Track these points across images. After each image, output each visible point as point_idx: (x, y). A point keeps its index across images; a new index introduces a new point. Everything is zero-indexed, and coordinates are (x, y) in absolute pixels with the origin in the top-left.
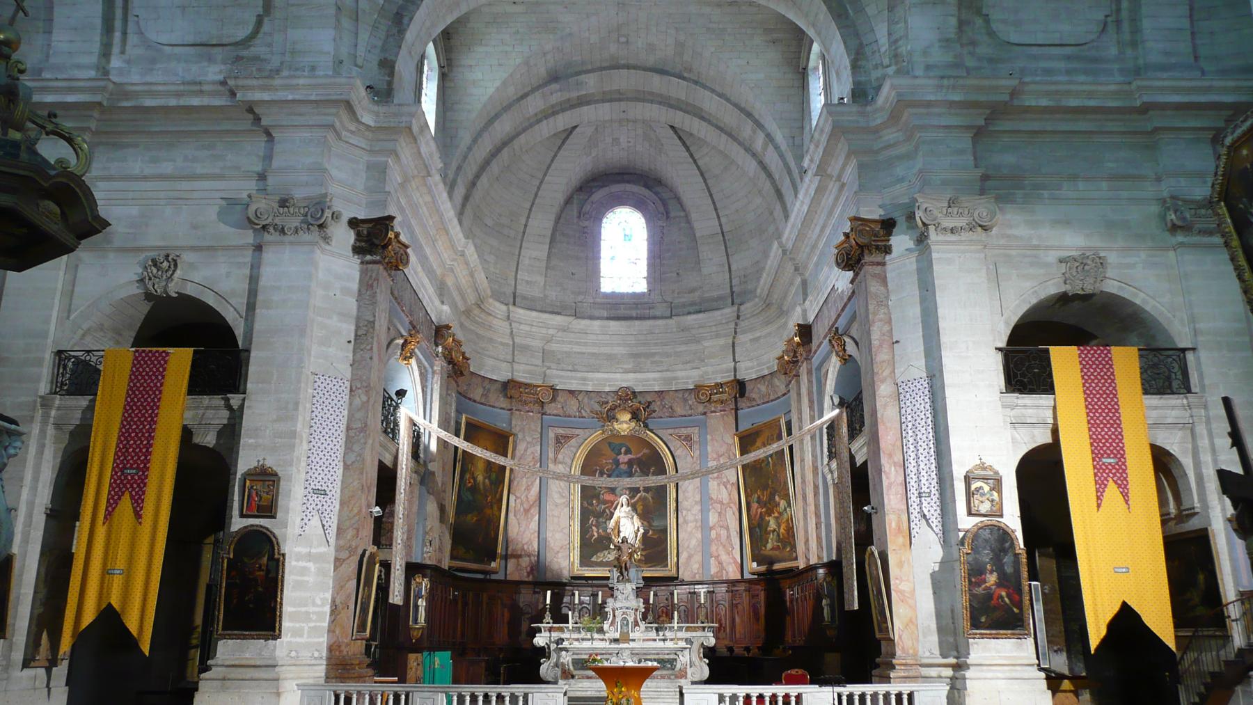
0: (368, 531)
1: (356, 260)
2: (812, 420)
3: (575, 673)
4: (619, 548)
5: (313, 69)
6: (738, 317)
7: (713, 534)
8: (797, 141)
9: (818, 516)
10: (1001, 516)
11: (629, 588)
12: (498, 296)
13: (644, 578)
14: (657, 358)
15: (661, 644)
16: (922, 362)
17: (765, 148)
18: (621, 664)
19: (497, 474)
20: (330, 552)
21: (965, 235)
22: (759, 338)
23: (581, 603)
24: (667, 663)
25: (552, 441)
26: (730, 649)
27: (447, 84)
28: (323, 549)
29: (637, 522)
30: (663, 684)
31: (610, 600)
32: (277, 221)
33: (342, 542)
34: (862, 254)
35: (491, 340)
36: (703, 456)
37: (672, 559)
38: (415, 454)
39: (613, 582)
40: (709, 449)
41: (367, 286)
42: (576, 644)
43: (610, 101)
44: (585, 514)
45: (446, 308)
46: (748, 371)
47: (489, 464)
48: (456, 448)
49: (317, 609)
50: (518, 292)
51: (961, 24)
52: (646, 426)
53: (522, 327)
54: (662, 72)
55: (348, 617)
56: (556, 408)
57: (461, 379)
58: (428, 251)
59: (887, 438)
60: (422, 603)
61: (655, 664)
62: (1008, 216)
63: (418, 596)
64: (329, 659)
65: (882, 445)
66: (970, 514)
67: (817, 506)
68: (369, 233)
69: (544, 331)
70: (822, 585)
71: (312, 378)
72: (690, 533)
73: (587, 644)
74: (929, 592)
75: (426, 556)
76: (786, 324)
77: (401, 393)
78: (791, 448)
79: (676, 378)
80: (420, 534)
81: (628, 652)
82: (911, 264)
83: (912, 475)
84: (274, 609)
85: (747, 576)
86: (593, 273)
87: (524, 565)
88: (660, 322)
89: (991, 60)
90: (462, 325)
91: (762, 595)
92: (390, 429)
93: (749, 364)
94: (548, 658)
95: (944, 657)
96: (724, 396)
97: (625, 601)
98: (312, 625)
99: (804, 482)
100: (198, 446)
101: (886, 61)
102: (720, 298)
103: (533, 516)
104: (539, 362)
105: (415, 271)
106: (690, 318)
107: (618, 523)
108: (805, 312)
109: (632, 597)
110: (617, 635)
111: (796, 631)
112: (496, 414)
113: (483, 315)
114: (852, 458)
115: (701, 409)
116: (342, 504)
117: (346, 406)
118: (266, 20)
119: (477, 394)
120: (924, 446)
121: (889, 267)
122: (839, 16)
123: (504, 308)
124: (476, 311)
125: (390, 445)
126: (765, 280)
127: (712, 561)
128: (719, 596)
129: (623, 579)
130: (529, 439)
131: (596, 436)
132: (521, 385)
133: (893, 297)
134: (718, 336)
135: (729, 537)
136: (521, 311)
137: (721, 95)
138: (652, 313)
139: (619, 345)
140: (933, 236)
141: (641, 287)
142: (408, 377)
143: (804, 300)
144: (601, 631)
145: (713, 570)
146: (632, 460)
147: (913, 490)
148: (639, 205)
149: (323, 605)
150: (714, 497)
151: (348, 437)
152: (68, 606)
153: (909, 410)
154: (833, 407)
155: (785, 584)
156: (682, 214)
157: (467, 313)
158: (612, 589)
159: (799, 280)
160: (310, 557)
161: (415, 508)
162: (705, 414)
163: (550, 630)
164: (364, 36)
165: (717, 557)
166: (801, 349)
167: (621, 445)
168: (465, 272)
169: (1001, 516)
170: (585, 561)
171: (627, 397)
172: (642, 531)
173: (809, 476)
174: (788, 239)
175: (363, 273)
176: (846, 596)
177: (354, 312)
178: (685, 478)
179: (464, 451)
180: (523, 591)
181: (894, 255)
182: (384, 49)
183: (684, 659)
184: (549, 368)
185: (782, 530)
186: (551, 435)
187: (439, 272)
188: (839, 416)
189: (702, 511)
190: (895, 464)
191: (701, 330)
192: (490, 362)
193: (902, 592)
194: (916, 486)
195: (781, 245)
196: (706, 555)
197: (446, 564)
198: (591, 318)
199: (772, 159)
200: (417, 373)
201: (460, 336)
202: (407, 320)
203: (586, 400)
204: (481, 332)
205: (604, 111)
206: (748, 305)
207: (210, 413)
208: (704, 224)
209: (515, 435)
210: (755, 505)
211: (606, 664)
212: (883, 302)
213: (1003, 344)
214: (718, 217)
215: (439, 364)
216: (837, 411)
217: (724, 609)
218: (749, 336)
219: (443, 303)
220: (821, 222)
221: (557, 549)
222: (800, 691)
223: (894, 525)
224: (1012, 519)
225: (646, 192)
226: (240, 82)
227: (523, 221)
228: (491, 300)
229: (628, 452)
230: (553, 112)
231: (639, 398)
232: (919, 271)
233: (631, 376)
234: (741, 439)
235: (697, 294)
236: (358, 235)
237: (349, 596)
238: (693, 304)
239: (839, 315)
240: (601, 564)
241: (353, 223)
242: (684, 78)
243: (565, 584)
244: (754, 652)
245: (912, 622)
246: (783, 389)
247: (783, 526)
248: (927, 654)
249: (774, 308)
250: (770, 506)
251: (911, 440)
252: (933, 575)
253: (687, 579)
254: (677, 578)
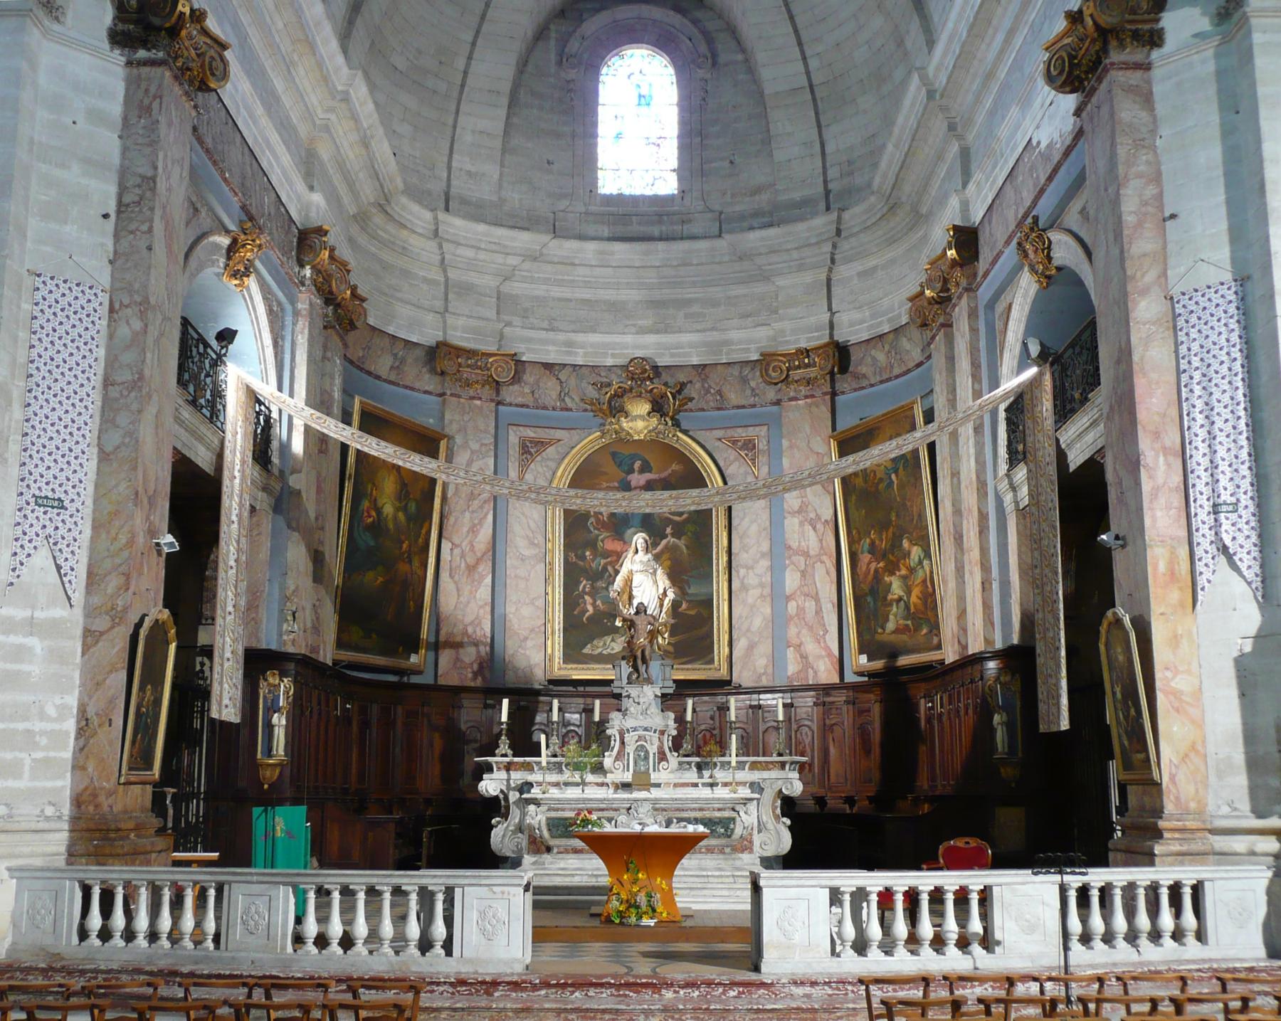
0: (152, 579)
1: (117, 58)
2: (977, 394)
3: (552, 842)
4: (630, 624)
6: (839, 232)
7: (792, 607)
9: (985, 568)
11: (649, 693)
13: (675, 681)
14: (696, 308)
15: (705, 793)
18: (638, 828)
19: (419, 493)
20: (74, 618)
22: (874, 269)
23: (566, 724)
24: (721, 826)
25: (514, 451)
26: (820, 801)
28: (60, 612)
29: (663, 582)
30: (710, 861)
31: (615, 717)
33: (96, 600)
34: (1105, 50)
35: (406, 273)
37: (721, 649)
39: (621, 685)
41: (140, 109)
42: (554, 793)
44: (572, 575)
45: (317, 198)
46: (853, 329)
48: (344, 448)
49: (49, 726)
50: (453, 191)
52: (677, 424)
53: (461, 251)
55: (112, 742)
56: (523, 395)
57: (351, 337)
58: (279, 85)
59: (1152, 402)
60: (279, 721)
61: (701, 829)
63: (273, 708)
64: (74, 820)
65: (1142, 415)
67: (984, 551)
69: (499, 259)
70: (992, 690)
71: (29, 281)
72: (752, 607)
73: (573, 793)
74: (1233, 692)
75: (288, 637)
76: (925, 238)
77: (227, 336)
78: (932, 447)
79: (727, 343)
80: (266, 596)
81: (646, 807)
82: (1205, 63)
83: (1200, 471)
85: (850, 678)
86: (586, 163)
87: (467, 660)
88: (702, 245)
90: (351, 240)
91: (876, 709)
92: (212, 408)
93: (856, 315)
94: (506, 816)
95: (1260, 816)
96: (812, 372)
97: (642, 716)
98: (39, 755)
99: (958, 512)
102: (805, 203)
103: (482, 578)
104: (491, 314)
105: (237, 90)
106: (753, 235)
107: (629, 582)
108: (965, 207)
109: (655, 709)
110: (628, 777)
111: (941, 764)
112: (418, 400)
113: (391, 228)
114: (1061, 456)
115: (771, 394)
116: (96, 527)
117: (102, 339)
119: (383, 365)
120: (1226, 414)
121: (1157, 73)
123: (428, 215)
124: (378, 219)
125: (205, 430)
126: (891, 157)
127: (790, 653)
129: (638, 677)
130: (475, 446)
131: (589, 442)
132: (459, 351)
133: (1165, 131)
134: (801, 268)
135: (819, 611)
136: (458, 222)
138: (687, 229)
141: (668, 185)
142: (246, 312)
143: (965, 185)
144: (599, 769)
145: (792, 668)
146: (651, 459)
147: (1202, 500)
148: (664, 42)
149: (61, 718)
150: (795, 545)
151: (106, 400)
153: (1195, 347)
154: (1024, 359)
156: (740, 57)
157: (361, 219)
158: (618, 697)
159: (954, 148)
161: (264, 553)
162: (778, 403)
163: (508, 767)
165: (799, 646)
166: (958, 273)
167: (634, 457)
168: (354, 137)
170: (573, 652)
171: (644, 376)
172: (671, 595)
173: (970, 499)
174: (938, 69)
175: (132, 84)
176: (1042, 707)
177: (116, 159)
179: (359, 453)
180: (466, 703)
183: (748, 818)
184: (508, 324)
185: (914, 599)
186: (513, 438)
187: (303, 130)
188: (1035, 383)
189: (772, 568)
190: (1165, 451)
191: (775, 258)
192: (404, 311)
193: (1176, 694)
194: (1207, 491)
195: (924, 79)
196: (780, 642)
197: (327, 654)
198: (582, 237)
200: (258, 298)
201: (344, 252)
202: (235, 201)
203: (573, 382)
206: (857, 210)
208: (778, 71)
209: (450, 438)
210: (865, 558)
211: (609, 828)
212: (1146, 142)
214: (804, 58)
215: (306, 300)
216: (1033, 370)
217: (808, 736)
218: (858, 266)
219: (311, 188)
220: (1007, 23)
221: (524, 633)
222: (988, 881)
223: (1162, 567)
225: (675, 19)
227: (460, 63)
228: (404, 200)
229: (645, 468)
231: (665, 377)
233: (651, 339)
235: (764, 197)
237: (111, 701)
239: (1041, 192)
243: (537, 693)
244: (862, 805)
245: (1195, 750)
246: (917, 355)
247: (916, 592)
248: (1225, 810)
249: (903, 210)
250: (892, 558)
251: (1199, 404)
252: (1242, 665)
254: (729, 682)
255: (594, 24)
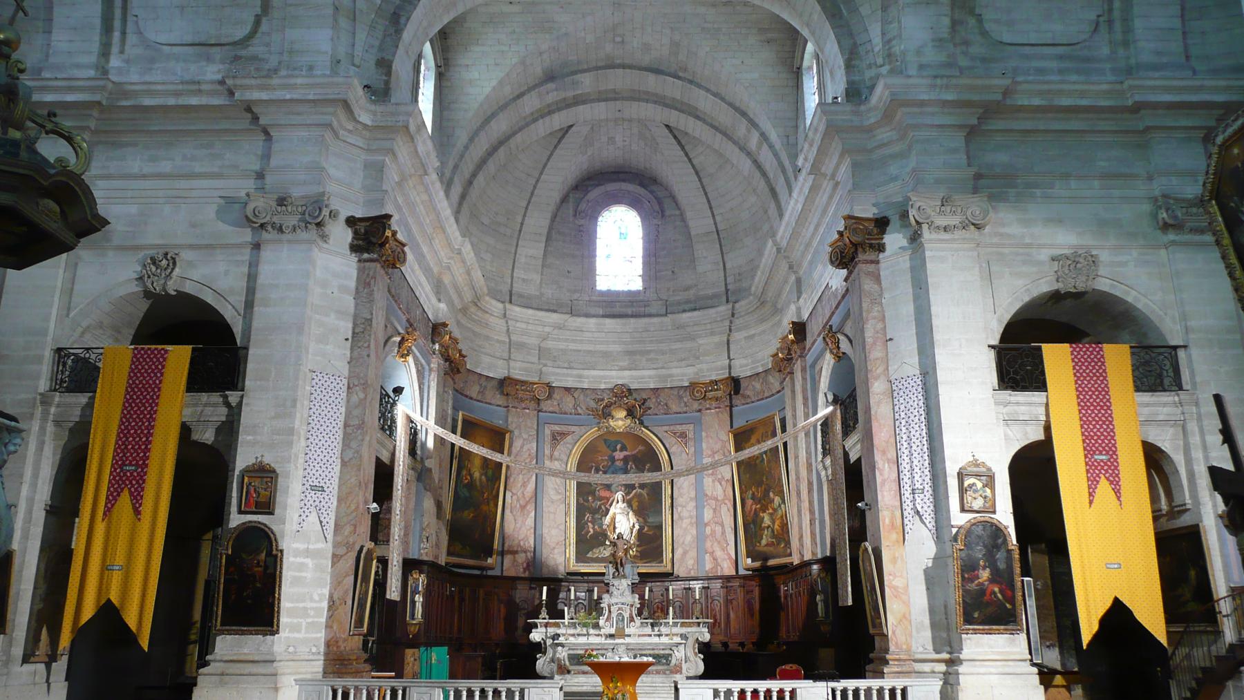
0: (365, 527)
1: (354, 258)
2: (807, 417)
3: (571, 668)
4: (614, 544)
5: (311, 68)
6: (733, 315)
7: (708, 530)
8: (792, 140)
9: (812, 512)
10: (994, 512)
11: (624, 584)
12: (494, 294)
13: (639, 574)
14: (652, 356)
15: (656, 640)
16: (915, 360)
17: (759, 147)
18: (617, 659)
19: (493, 471)
20: (328, 548)
21: (959, 234)
22: (754, 335)
23: (577, 598)
24: (662, 659)
25: (548, 438)
26: (725, 645)
27: (444, 84)
28: (321, 545)
29: (633, 518)
30: (658, 679)
31: (606, 596)
32: (275, 219)
33: (339, 539)
34: (856, 252)
35: (487, 338)
36: (698, 453)
37: (667, 555)
38: (412, 451)
39: (609, 578)
40: (704, 445)
41: (364, 284)
42: (572, 640)
43: (606, 100)
44: (581, 511)
45: (442, 306)
46: (742, 369)
47: (485, 461)
48: (453, 445)
49: (314, 605)
50: (515, 290)
51: (954, 24)
52: (641, 423)
53: (518, 325)
54: (657, 71)
55: (346, 613)
56: (552, 406)
57: (457, 377)
58: (425, 249)
59: (881, 435)
60: (419, 599)
61: (651, 659)
62: (1001, 215)
63: (415, 592)
64: (326, 654)
65: (876, 441)
66: (963, 510)
67: (811, 502)
68: (366, 232)
69: (540, 328)
70: (816, 581)
71: (309, 375)
72: (685, 529)
73: (582, 640)
74: (922, 587)
75: (423, 552)
76: (780, 321)
77: (398, 391)
78: (785, 444)
79: (671, 376)
80: (417, 530)
81: (623, 647)
82: (905, 262)
83: (905, 472)
84: (273, 605)
85: (742, 572)
86: (589, 272)
87: (520, 561)
88: (655, 320)
89: (984, 60)
90: (458, 323)
91: (757, 591)
92: (388, 426)
93: (744, 362)
94: (545, 653)
95: (937, 653)
96: (719, 394)
97: (621, 596)
98: (310, 620)
99: (798, 478)
100: (196, 443)
101: (880, 61)
102: (715, 296)
103: (529, 512)
104: (535, 360)
105: (412, 269)
106: (685, 315)
107: (613, 519)
108: (799, 309)
109: (628, 593)
110: (613, 631)
111: (790, 627)
112: (493, 411)
113: (479, 313)
114: (846, 455)
115: (696, 406)
116: (339, 500)
117: (343, 403)
118: (264, 20)
119: (474, 391)
120: (918, 442)
121: (882, 265)
122: (833, 16)
123: (500, 306)
124: (473, 309)
125: (387, 442)
126: (760, 278)
127: (707, 557)
128: (714, 592)
129: (618, 575)
130: (525, 436)
131: (591, 433)
132: (517, 382)
133: (886, 295)
134: (712, 334)
135: (723, 533)
136: (518, 309)
137: (716, 95)
138: (648, 310)
139: (614, 343)
140: (926, 234)
141: (637, 285)
142: (405, 374)
143: (799, 298)
144: (596, 626)
145: (708, 566)
146: (628, 457)
147: (907, 487)
148: (634, 204)
149: (320, 601)
150: (709, 494)
151: (345, 434)
152: (68, 602)
153: (902, 407)
154: (827, 404)
155: (779, 580)
156: (677, 212)
157: (464, 310)
158: (607, 585)
159: (793, 278)
160: (307, 553)
161: (412, 505)
162: (700, 411)
163: (546, 625)
164: (361, 36)
165: (712, 553)
166: (795, 346)
167: (617, 442)
168: (462, 270)
169: (994, 512)
170: (581, 557)
171: (622, 394)
172: (637, 527)
173: (804, 473)
174: (782, 238)
175: (361, 271)
176: (840, 592)
177: (352, 310)
178: (680, 474)
179: (461, 448)
180: (519, 587)
181: (887, 253)
182: (381, 49)
183: (679, 654)
184: (545, 365)
185: (776, 527)
186: (547, 432)
187: (436, 270)
188: (833, 413)
189: (697, 507)
190: (889, 461)
191: (696, 328)
192: (486, 360)
193: (895, 588)
194: (909, 482)
195: (775, 243)
196: (701, 551)
197: (443, 560)
198: (587, 316)
199: (766, 157)
200: (414, 370)
201: (457, 333)
202: (404, 318)
203: (582, 397)
204: (477, 329)
205: (599, 111)
206: (743, 303)
207: (208, 410)
208: (699, 223)
209: (511, 432)
210: (749, 502)
211: (602, 659)
212: (877, 300)
213: (995, 342)
214: (713, 216)
215: (436, 362)
216: (831, 408)
217: (718, 605)
218: (744, 334)
219: (439, 300)
220: (815, 221)
221: (553, 545)
222: (794, 686)
223: (887, 521)
224: (1005, 515)
225: (642, 191)
226: (238, 82)
227: (519, 219)
228: (487, 298)
229: (623, 448)
230: (549, 111)
231: (635, 395)
232: (913, 269)
233: (627, 373)
234: (735, 436)
235: (692, 292)
236: (356, 233)
237: (346, 592)
238: (688, 302)
239: (833, 313)
240: (597, 560)
241: (351, 221)
242: (679, 78)
243: (561, 580)
244: (749, 647)
245: (905, 618)
246: (777, 386)
247: (777, 523)
248: (921, 649)
249: (768, 306)
250: (764, 502)
251: (905, 437)
252: (926, 571)
253: (682, 575)
254: (672, 574)
255: (595, 193)
